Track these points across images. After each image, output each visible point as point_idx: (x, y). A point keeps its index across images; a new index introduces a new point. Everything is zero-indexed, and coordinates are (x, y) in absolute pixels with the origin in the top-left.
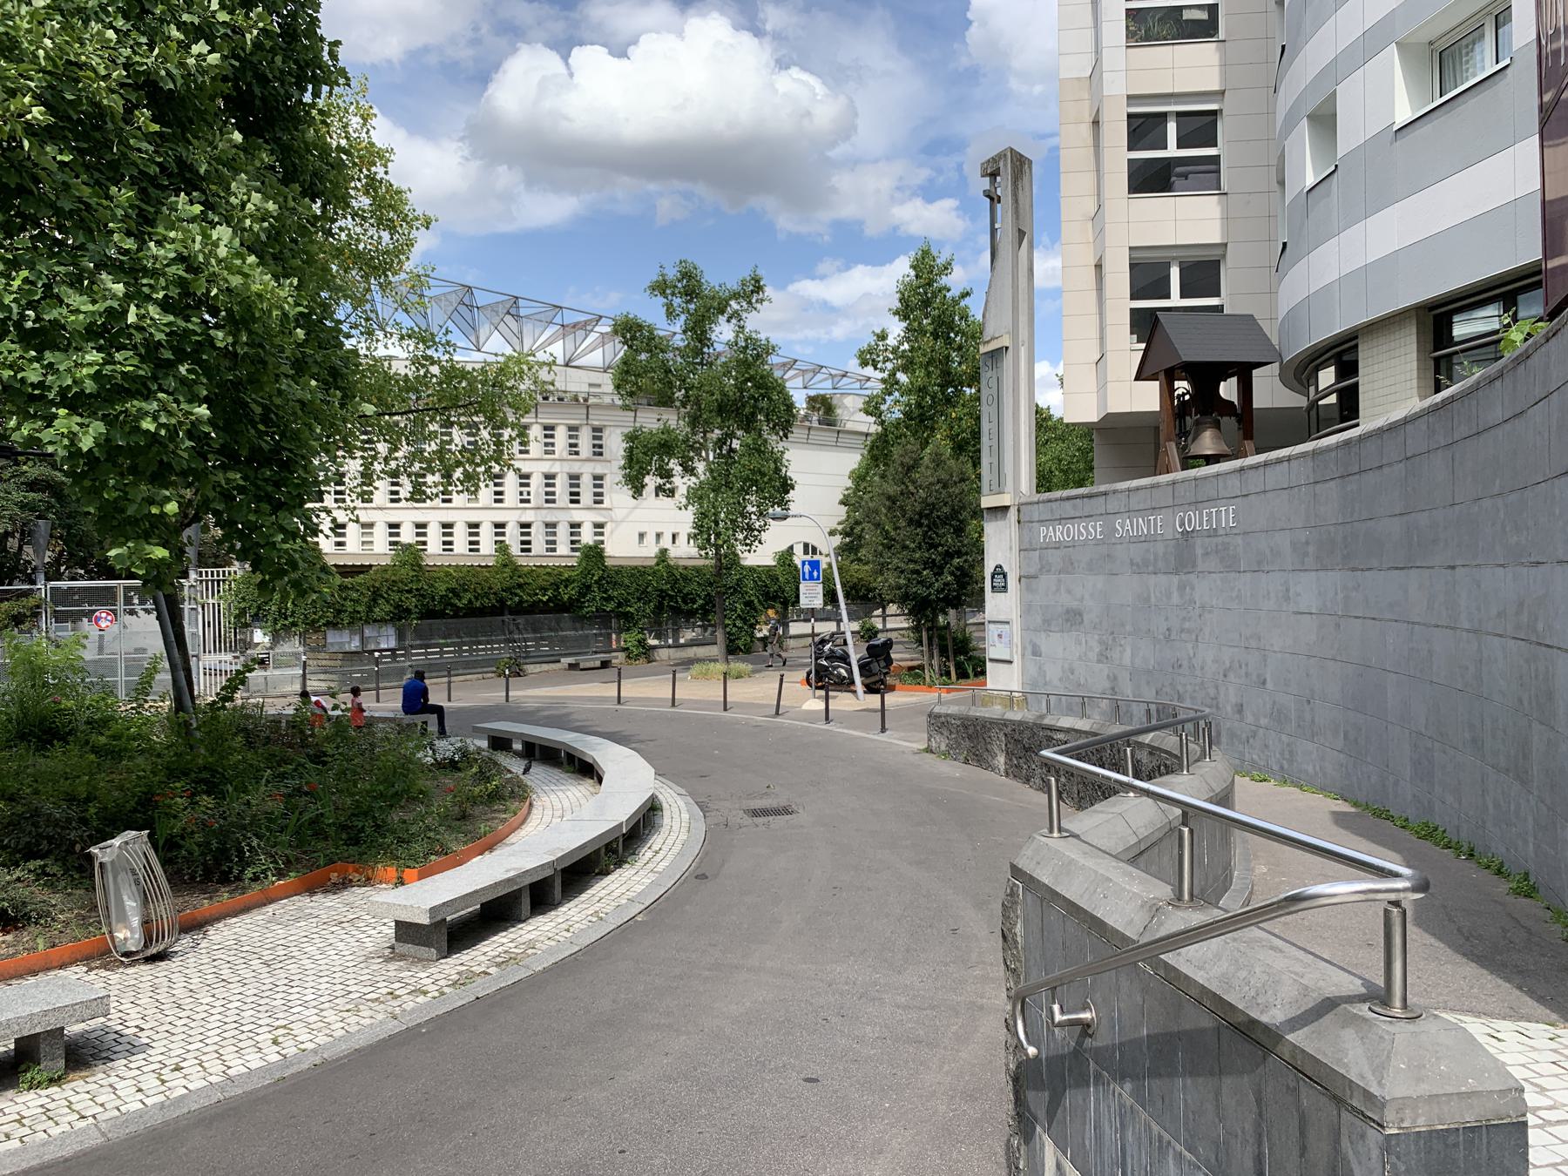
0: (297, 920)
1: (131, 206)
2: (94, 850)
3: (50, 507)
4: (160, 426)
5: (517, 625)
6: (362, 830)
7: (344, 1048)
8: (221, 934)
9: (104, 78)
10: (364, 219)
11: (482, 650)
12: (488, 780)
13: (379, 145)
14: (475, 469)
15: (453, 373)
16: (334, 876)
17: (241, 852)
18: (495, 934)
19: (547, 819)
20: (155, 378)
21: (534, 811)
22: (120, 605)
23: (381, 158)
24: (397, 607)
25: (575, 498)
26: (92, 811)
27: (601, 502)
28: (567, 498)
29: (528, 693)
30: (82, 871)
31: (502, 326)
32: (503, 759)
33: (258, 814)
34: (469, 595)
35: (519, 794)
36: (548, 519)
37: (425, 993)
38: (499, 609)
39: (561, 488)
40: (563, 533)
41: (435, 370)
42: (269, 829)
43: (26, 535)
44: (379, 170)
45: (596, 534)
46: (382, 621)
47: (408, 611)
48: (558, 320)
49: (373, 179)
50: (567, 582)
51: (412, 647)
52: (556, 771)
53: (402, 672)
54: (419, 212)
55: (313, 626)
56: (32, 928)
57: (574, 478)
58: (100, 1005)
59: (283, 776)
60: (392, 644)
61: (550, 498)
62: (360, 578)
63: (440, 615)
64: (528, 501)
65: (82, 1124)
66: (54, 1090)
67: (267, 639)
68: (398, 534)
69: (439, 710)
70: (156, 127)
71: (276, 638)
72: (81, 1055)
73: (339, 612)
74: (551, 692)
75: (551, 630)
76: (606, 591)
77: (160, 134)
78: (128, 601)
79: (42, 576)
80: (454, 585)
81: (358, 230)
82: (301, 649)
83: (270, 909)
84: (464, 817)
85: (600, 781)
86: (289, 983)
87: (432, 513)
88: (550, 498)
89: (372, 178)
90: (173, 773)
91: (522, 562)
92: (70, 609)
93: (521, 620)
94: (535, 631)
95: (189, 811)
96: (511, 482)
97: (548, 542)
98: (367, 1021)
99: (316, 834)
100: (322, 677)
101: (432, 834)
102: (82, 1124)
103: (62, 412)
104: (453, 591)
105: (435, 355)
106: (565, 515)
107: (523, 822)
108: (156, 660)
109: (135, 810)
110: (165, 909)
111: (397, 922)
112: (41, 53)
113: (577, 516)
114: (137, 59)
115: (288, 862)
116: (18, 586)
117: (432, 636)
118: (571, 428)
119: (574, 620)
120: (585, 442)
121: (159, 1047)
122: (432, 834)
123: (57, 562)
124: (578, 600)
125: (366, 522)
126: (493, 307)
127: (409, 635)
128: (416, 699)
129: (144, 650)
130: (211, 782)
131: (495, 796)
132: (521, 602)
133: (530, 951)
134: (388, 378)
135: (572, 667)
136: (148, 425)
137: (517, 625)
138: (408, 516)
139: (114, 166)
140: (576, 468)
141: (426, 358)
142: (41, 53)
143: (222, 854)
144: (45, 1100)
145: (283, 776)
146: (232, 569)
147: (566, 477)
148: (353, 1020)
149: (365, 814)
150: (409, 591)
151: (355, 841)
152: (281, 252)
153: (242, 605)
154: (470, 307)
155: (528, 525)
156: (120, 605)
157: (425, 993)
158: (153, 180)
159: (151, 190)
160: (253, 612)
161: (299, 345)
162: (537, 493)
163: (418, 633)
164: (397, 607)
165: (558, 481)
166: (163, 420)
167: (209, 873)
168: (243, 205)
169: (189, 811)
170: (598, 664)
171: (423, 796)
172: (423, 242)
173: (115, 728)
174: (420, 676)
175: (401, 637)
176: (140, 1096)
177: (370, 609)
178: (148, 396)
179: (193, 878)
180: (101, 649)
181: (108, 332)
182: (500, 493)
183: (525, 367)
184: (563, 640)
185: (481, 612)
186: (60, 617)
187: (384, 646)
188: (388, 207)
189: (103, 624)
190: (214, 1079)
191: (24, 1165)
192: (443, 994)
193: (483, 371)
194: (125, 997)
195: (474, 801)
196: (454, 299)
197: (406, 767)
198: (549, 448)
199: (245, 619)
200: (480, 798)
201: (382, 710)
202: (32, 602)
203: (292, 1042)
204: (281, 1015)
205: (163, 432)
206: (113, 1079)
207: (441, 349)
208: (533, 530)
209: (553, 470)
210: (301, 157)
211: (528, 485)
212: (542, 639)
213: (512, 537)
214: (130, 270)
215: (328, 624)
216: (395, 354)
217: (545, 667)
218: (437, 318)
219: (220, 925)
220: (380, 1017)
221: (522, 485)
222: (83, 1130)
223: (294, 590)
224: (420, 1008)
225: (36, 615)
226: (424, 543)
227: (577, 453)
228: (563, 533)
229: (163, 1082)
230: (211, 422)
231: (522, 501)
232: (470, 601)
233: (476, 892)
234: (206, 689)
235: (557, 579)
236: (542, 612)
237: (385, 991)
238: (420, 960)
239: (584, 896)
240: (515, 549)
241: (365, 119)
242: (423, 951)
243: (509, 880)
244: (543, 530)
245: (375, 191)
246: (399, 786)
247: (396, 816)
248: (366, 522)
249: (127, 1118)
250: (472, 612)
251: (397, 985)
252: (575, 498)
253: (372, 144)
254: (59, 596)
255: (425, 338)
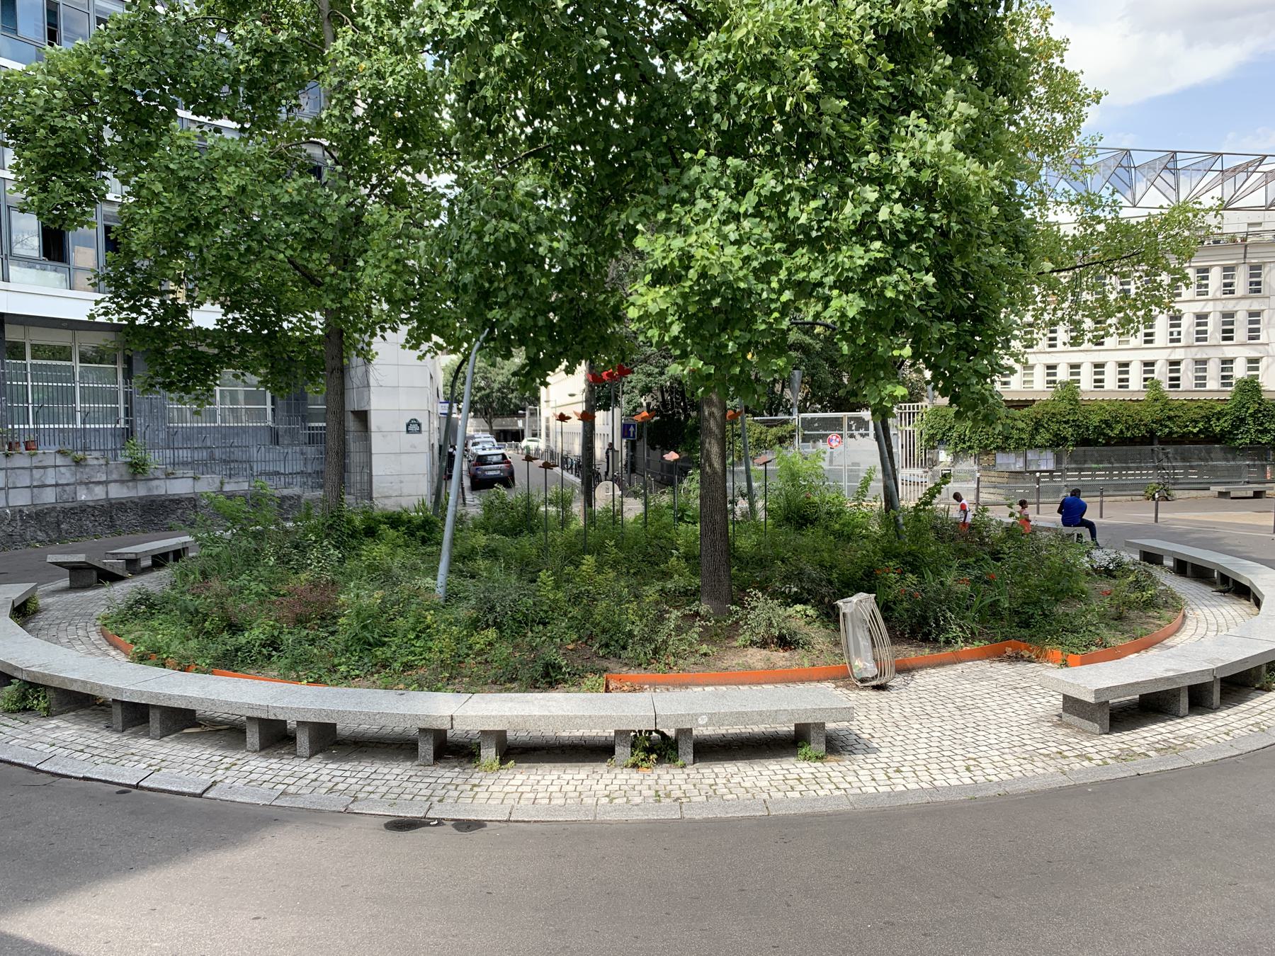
0: (981, 679)
1: (875, 132)
2: (840, 603)
3: (802, 361)
4: (899, 292)
5: (1166, 455)
6: (1032, 616)
7: (1022, 787)
8: (926, 678)
9: (857, 42)
10: (1040, 106)
11: (1131, 476)
12: (1143, 589)
13: (1055, 39)
14: (1134, 315)
15: (1120, 229)
16: (1009, 650)
17: (937, 621)
18: (1154, 722)
19: (1201, 631)
20: (894, 256)
21: (1188, 622)
22: (845, 432)
23: (1057, 49)
24: (1056, 435)
25: (1228, 335)
26: (835, 575)
27: (1258, 338)
28: (1219, 335)
29: (1172, 516)
30: (831, 616)
31: (1159, 182)
32: (1156, 571)
33: (954, 594)
34: (1120, 426)
35: (1173, 604)
36: (1198, 357)
37: (1090, 759)
38: (1149, 439)
39: (1213, 326)
40: (1213, 370)
41: (1101, 228)
42: (959, 606)
43: (786, 383)
44: (1056, 61)
45: (1250, 369)
46: (1042, 447)
47: (1065, 439)
48: (1218, 166)
49: (1051, 69)
50: (1220, 415)
51: (1068, 470)
52: (1209, 589)
53: (1058, 490)
54: (1091, 90)
55: (985, 450)
56: (800, 650)
57: (1228, 317)
58: (848, 714)
59: (966, 566)
60: (1051, 466)
61: (1201, 336)
62: (1025, 411)
63: (1095, 443)
64: (1179, 340)
65: (837, 793)
66: (818, 764)
67: (949, 459)
68: (1055, 374)
69: (1091, 526)
70: (892, 66)
71: (956, 457)
72: (836, 746)
73: (1007, 438)
74: (1198, 516)
75: (1201, 459)
76: (1261, 425)
77: (892, 72)
78: (850, 427)
79: (796, 410)
80: (1107, 417)
81: (1035, 116)
82: (976, 468)
83: (959, 667)
84: (1120, 618)
85: (1258, 603)
86: (966, 729)
87: (1086, 356)
88: (1201, 336)
89: (1049, 69)
90: (888, 554)
91: (1172, 396)
92: (814, 432)
93: (1170, 449)
94: (1184, 460)
95: (903, 585)
96: (1162, 323)
97: (1197, 378)
98: (1041, 771)
99: (994, 614)
100: (992, 490)
101: (1093, 628)
102: (837, 793)
103: (835, 292)
104: (1106, 422)
105: (1102, 215)
106: (1215, 352)
107: (1178, 630)
108: (871, 472)
109: (862, 579)
110: (887, 652)
111: (1065, 697)
112: (817, 33)
113: (1229, 352)
114: (885, 16)
115: (973, 633)
116: (781, 416)
117: (1085, 462)
118: (1226, 269)
119: (1225, 451)
120: (1241, 281)
121: (885, 753)
122: (1093, 628)
123: (805, 400)
124: (1230, 432)
125: (1041, 364)
126: (1150, 165)
127: (1065, 460)
128: (1072, 511)
129: (858, 464)
130: (913, 564)
131: (1150, 604)
132: (1171, 433)
133: (1189, 745)
134: (1059, 240)
135: (1222, 495)
136: (890, 294)
137: (1166, 455)
138: (1063, 358)
139: (863, 103)
140: (1230, 306)
141: (1093, 218)
142: (817, 33)
143: (924, 620)
144: (813, 770)
145: (966, 566)
146: (924, 404)
147: (1218, 315)
148: (1029, 767)
149: (1035, 604)
150: (1066, 422)
151: (1027, 625)
152: (977, 146)
153: (932, 432)
154: (1128, 169)
155: (1177, 363)
156: (845, 432)
157: (1090, 759)
158: (889, 110)
159: (887, 115)
160: (939, 437)
161: (993, 219)
162: (1188, 333)
163: (1073, 458)
164: (1056, 435)
165: (1210, 320)
166: (901, 287)
167: (916, 629)
168: (951, 114)
169: (903, 585)
170: (1251, 494)
171: (1080, 596)
172: (1092, 115)
173: (846, 517)
174: (1076, 493)
175: (1058, 461)
176: (874, 783)
177: (1032, 437)
178: (889, 272)
179: (902, 634)
180: (831, 462)
181: (865, 229)
182: (1151, 334)
183: (1190, 215)
184: (1213, 470)
185: (1132, 441)
186: (805, 439)
187: (1043, 468)
188: (1066, 93)
189: (834, 444)
190: (924, 785)
191: (803, 811)
192: (1106, 763)
193: (1148, 222)
194: (861, 712)
195: (1130, 605)
196: (1113, 163)
197: (1068, 571)
198: (1202, 289)
199: (935, 440)
200: (1136, 607)
201: (1042, 520)
202: (790, 428)
203: (980, 773)
204: (971, 750)
205: (901, 298)
206: (856, 767)
207: (1107, 209)
208: (1182, 367)
209: (1206, 310)
210: (995, 64)
211: (1179, 326)
212: (1192, 467)
213: (1161, 373)
214: (880, 179)
215: (997, 448)
216: (1065, 221)
217: (1194, 493)
218: (1095, 183)
219: (923, 672)
220: (1051, 770)
221: (1172, 326)
222: (839, 797)
223: (979, 420)
224: (1086, 771)
225: (792, 437)
226: (1078, 381)
227: (1232, 292)
228: (1213, 370)
229: (889, 778)
230: (934, 285)
231: (1172, 341)
232: (1121, 431)
233: (1137, 683)
234: (909, 498)
235: (1210, 413)
236: (1192, 442)
237: (1055, 750)
238: (1085, 731)
239: (1243, 707)
240: (1165, 386)
241: (1044, 20)
242: (1087, 724)
243: (1168, 679)
244: (1192, 366)
245: (1051, 79)
246: (1062, 586)
247: (1060, 609)
248: (1041, 364)
249: (865, 797)
250: (1123, 441)
251: (1064, 748)
252: (1228, 335)
253: (1050, 39)
254: (807, 424)
255: (1090, 201)
